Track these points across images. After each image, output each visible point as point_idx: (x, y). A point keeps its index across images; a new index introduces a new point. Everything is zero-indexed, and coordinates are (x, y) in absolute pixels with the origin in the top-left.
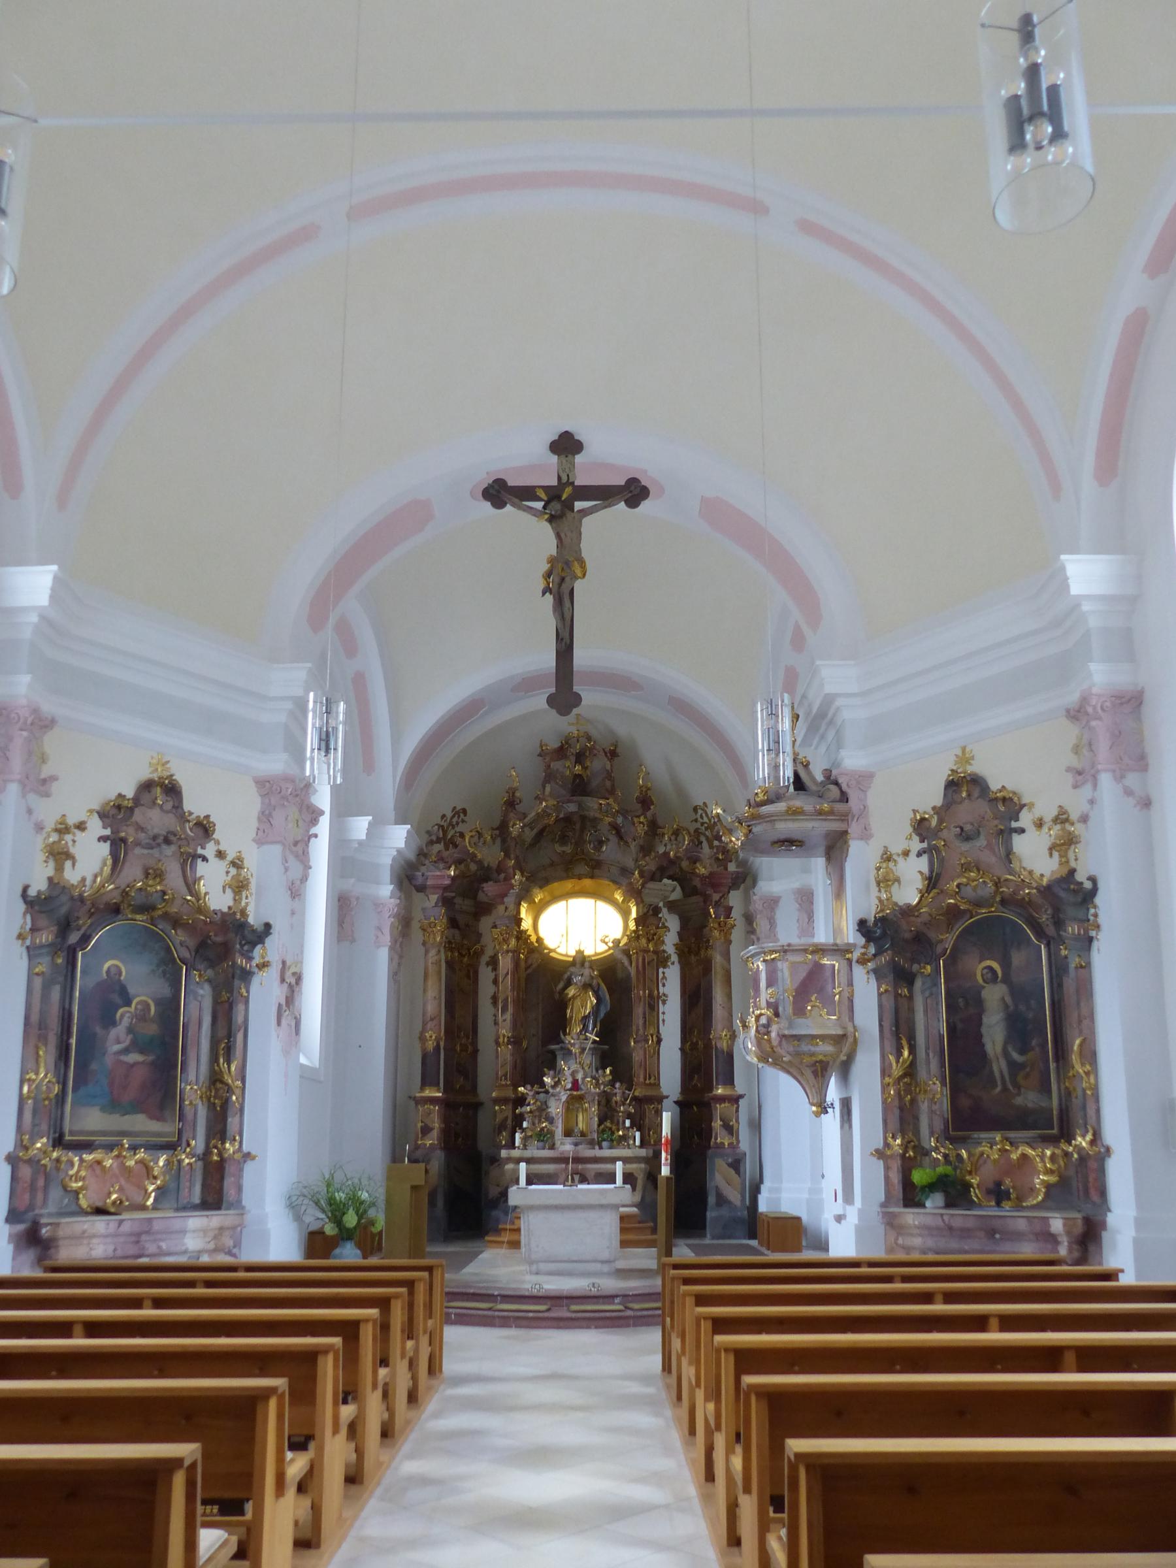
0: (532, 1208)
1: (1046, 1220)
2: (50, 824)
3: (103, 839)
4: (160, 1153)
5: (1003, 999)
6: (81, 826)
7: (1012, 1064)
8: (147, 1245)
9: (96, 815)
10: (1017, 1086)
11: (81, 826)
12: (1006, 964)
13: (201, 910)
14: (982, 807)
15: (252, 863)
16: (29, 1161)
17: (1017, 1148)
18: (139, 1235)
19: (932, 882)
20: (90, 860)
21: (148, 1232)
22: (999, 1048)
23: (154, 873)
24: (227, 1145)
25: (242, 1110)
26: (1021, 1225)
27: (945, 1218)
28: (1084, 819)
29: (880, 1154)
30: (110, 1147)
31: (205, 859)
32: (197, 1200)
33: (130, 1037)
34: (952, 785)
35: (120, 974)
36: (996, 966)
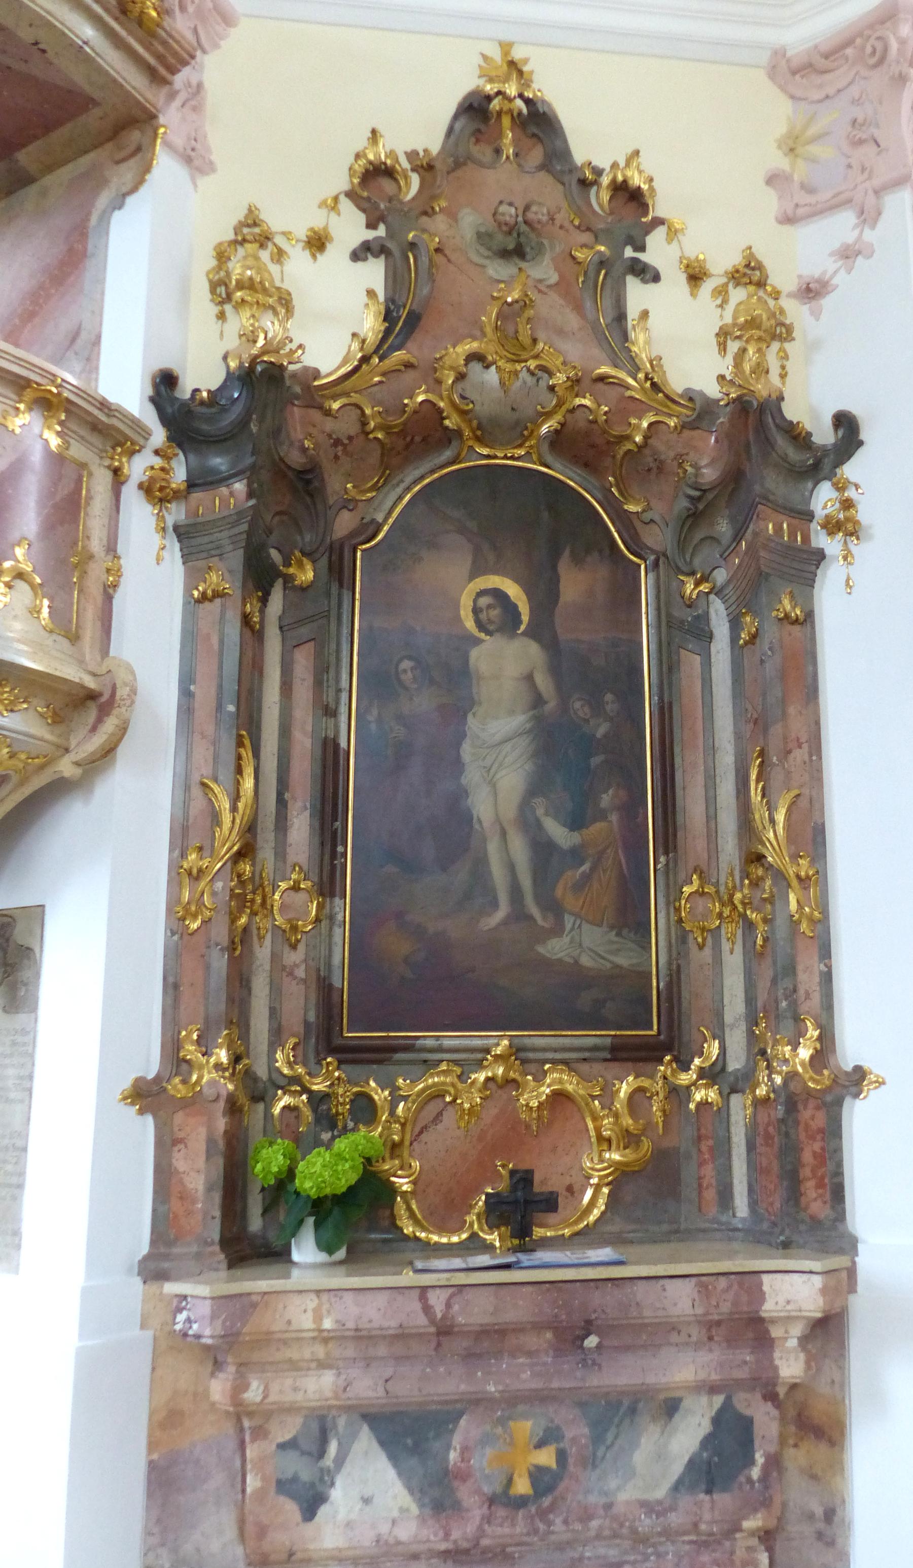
1: (749, 1281)
3: (361, 253)
5: (529, 678)
7: (543, 851)
10: (554, 908)
12: (545, 595)
14: (547, 196)
17: (539, 1078)
19: (402, 319)
20: (331, 317)
22: (509, 811)
26: (681, 1300)
27: (437, 1300)
28: (812, 291)
29: (144, 1095)
34: (476, 110)
36: (513, 590)
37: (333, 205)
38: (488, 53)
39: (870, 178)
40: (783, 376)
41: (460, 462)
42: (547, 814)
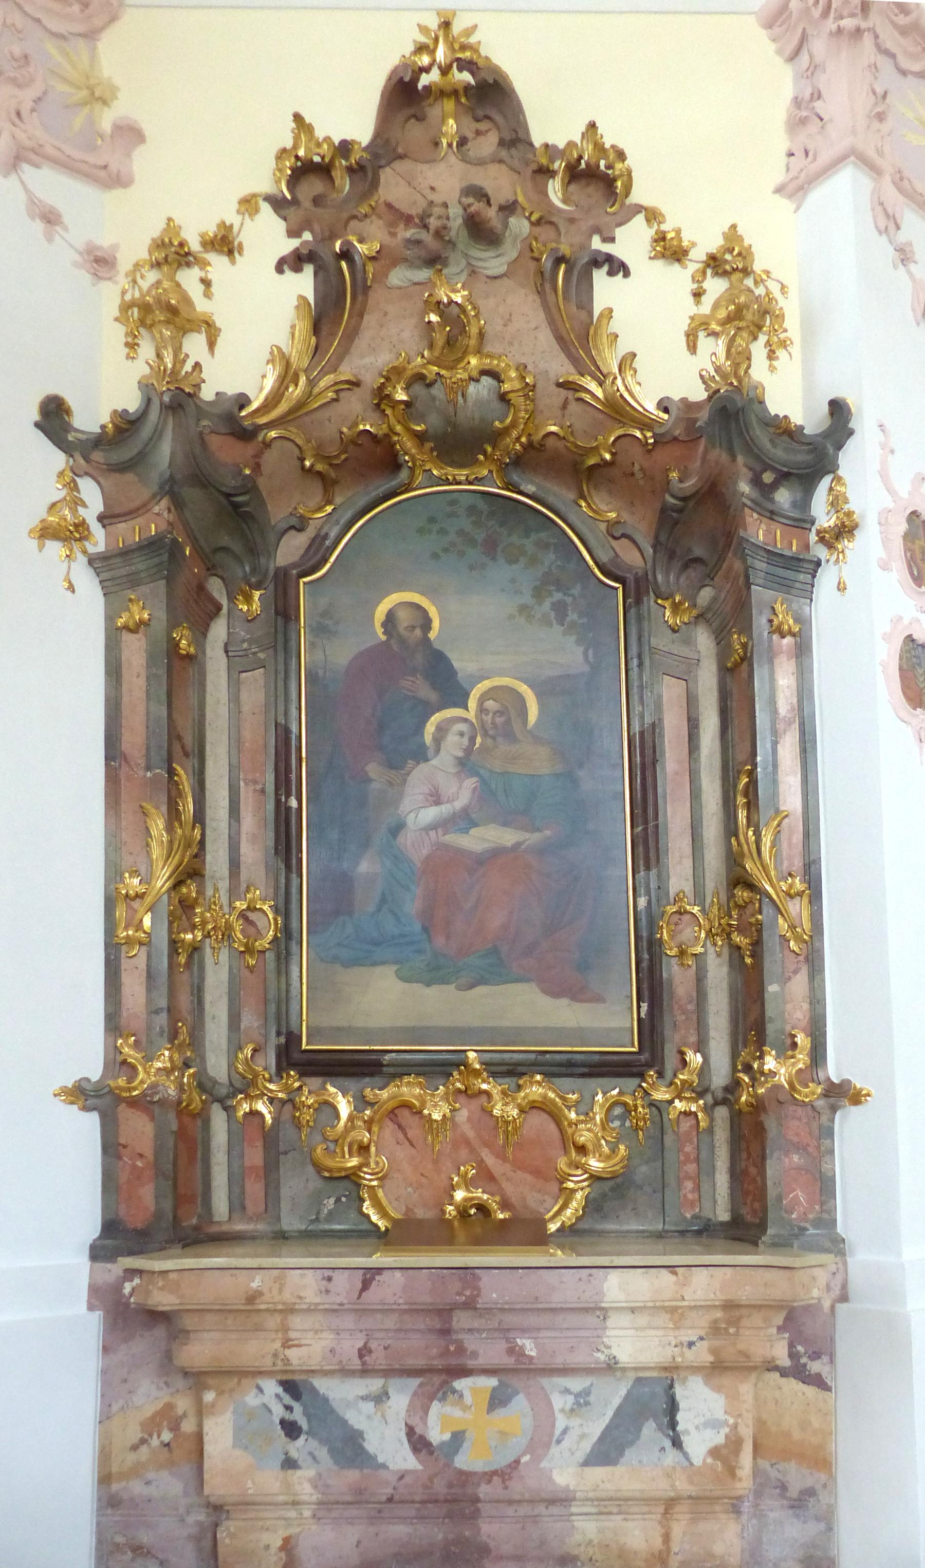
0: (462, 10)
2: (134, 248)
3: (293, 262)
4: (593, 1082)
6: (225, 243)
8: (471, 1343)
9: (266, 208)
11: (225, 243)
13: (618, 410)
15: (782, 248)
16: (140, 1103)
18: (444, 1312)
20: (253, 330)
21: (470, 1305)
23: (454, 333)
24: (770, 1063)
25: (813, 961)
30: (438, 1069)
31: (617, 267)
32: (724, 1216)
33: (471, 783)
35: (427, 624)
37: (248, 204)
38: (424, 23)
39: (815, 159)
40: (293, 327)
41: (415, 489)
42: (545, 1096)
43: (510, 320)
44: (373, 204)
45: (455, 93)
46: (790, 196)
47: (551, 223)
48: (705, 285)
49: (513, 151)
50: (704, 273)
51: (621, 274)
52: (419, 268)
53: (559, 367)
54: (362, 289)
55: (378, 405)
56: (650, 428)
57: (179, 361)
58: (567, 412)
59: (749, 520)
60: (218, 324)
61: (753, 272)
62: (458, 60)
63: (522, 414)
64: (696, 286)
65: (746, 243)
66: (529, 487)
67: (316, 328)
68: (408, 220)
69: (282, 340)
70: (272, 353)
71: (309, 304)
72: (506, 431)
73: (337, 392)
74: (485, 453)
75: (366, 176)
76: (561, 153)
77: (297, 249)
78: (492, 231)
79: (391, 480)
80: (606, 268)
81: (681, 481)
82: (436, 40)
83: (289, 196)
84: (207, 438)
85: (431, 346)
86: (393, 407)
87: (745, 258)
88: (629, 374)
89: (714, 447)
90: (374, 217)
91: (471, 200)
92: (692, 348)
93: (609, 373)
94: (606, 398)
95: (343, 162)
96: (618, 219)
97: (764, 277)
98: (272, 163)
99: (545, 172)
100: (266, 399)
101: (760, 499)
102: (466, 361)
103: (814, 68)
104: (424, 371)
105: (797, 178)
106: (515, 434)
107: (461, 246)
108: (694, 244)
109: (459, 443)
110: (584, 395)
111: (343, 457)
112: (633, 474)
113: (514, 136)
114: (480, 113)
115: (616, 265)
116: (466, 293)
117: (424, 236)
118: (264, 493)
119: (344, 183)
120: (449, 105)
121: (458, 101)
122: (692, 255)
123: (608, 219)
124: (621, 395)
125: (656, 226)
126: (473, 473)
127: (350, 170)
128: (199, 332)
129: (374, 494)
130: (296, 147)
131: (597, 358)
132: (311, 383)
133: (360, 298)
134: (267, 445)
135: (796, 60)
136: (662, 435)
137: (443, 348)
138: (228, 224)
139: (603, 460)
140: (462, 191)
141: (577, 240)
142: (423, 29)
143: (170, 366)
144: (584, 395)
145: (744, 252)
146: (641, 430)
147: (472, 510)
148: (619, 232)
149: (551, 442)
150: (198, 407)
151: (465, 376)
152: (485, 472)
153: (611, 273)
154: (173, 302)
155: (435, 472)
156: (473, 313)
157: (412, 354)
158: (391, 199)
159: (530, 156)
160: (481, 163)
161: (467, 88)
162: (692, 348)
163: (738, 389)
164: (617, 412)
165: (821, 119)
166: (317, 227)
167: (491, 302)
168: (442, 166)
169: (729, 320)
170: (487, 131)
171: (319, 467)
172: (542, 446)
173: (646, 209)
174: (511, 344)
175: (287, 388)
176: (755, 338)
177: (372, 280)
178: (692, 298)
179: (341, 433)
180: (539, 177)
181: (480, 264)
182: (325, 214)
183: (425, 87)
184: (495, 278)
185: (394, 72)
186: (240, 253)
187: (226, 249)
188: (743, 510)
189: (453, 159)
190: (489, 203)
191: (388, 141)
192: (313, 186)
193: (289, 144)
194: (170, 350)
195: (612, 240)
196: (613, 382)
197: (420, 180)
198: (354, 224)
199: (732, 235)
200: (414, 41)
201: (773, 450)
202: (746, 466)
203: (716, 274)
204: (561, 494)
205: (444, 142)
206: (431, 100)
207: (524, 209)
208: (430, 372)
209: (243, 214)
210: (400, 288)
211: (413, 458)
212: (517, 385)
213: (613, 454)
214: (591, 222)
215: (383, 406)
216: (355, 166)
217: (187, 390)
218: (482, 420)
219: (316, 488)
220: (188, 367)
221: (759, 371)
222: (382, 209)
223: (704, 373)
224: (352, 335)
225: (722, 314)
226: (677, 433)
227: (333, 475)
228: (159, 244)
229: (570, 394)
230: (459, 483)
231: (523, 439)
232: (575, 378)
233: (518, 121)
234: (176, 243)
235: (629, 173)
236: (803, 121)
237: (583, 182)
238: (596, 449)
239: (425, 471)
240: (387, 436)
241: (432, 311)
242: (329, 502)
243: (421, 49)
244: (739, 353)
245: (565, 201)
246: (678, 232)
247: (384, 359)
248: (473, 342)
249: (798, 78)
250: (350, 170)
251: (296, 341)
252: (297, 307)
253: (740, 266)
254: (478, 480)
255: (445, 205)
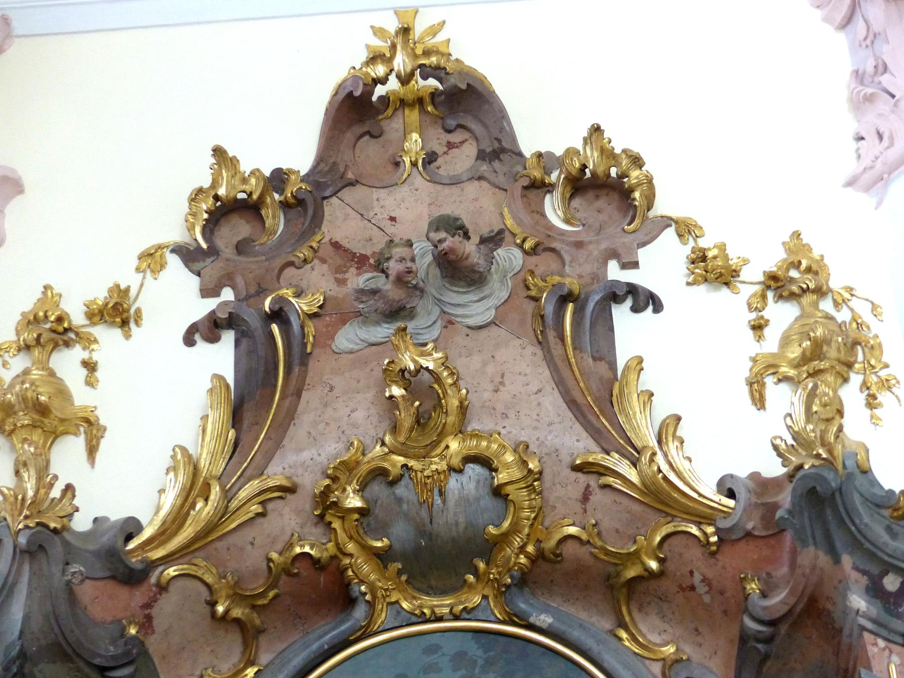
3: (209, 329)
6: (118, 312)
9: (174, 262)
11: (118, 312)
13: (662, 498)
23: (425, 407)
31: (645, 300)
37: (151, 260)
39: (891, 144)
40: (205, 418)
43: (502, 383)
44: (314, 245)
45: (420, 101)
46: (868, 189)
47: (552, 250)
48: (766, 314)
49: (496, 164)
50: (764, 297)
51: (651, 308)
52: (377, 323)
53: (577, 444)
54: (299, 358)
55: (322, 517)
56: (711, 521)
57: (45, 479)
58: (589, 506)
59: (872, 650)
60: (102, 422)
61: (831, 291)
62: (421, 66)
63: (526, 513)
64: (753, 315)
65: (816, 254)
66: (542, 617)
67: (236, 417)
68: (361, 261)
69: (189, 439)
70: (174, 457)
71: (228, 386)
72: (505, 538)
73: (261, 503)
74: (475, 572)
75: (306, 211)
76: (559, 162)
77: (213, 312)
78: (472, 270)
79: (342, 622)
80: (629, 302)
81: (764, 595)
82: (393, 47)
83: (204, 246)
84: (76, 589)
85: (395, 429)
86: (342, 518)
87: (816, 273)
88: (672, 446)
89: (805, 544)
90: (316, 261)
91: (442, 235)
92: (759, 401)
93: (645, 447)
94: (643, 483)
95: (276, 196)
96: (641, 237)
97: (847, 295)
98: (185, 207)
99: (539, 187)
100: (164, 523)
101: (886, 618)
102: (443, 445)
103: (873, 38)
104: (386, 465)
105: (872, 168)
106: (517, 541)
107: (431, 290)
108: (746, 262)
109: (437, 561)
110: (610, 480)
111: (271, 594)
112: (693, 588)
113: (496, 145)
114: (452, 123)
115: (642, 298)
116: (440, 355)
117: (380, 282)
118: (156, 660)
119: (276, 222)
120: (413, 116)
121: (422, 110)
122: (744, 275)
123: (627, 239)
124: (665, 478)
125: (691, 243)
126: (461, 603)
127: (285, 205)
128: (76, 434)
129: (315, 647)
130: (215, 184)
131: (626, 427)
132: (228, 495)
133: (296, 369)
134: (162, 588)
135: (849, 27)
136: (730, 530)
137: (411, 430)
138: (122, 287)
139: (647, 569)
140: (430, 224)
141: (588, 269)
142: (378, 32)
143: (30, 493)
144: (610, 480)
145: (815, 267)
146: (698, 524)
147: (459, 659)
148: (643, 255)
149: (570, 549)
150: (66, 543)
151: (443, 466)
152: (477, 599)
153: (636, 309)
154: (43, 398)
155: (405, 605)
156: (450, 381)
157: (368, 441)
158: (338, 237)
159: (519, 168)
160: (455, 182)
161: (434, 95)
162: (759, 401)
163: (829, 463)
164: (663, 502)
165: (893, 96)
166: (240, 281)
167: (476, 361)
168: (403, 191)
169: (805, 359)
170: (463, 142)
171: (237, 613)
172: (557, 556)
173: (676, 222)
174: (505, 416)
175: (193, 506)
176: (846, 380)
177: (313, 345)
178: (751, 332)
179: (270, 560)
180: (532, 194)
181: (459, 311)
182: (251, 265)
183: (381, 98)
184: (480, 328)
185: (340, 86)
186: (137, 324)
187: (118, 320)
188: (861, 636)
189: (419, 181)
190: (467, 236)
191: (335, 164)
192: (237, 229)
193: (206, 183)
194: (32, 472)
195: (635, 265)
196: (652, 460)
197: (377, 210)
198: (290, 272)
199: (796, 245)
200: (368, 47)
201: (893, 544)
202: (856, 568)
203: (780, 297)
204: (591, 621)
205: (407, 160)
206: (390, 111)
207: (514, 235)
208: (394, 465)
209: (144, 271)
210: (351, 352)
211: (373, 589)
212: (517, 474)
213: (661, 561)
214: (604, 245)
215: (328, 518)
216: (292, 201)
217: (52, 525)
218: (470, 525)
219: (233, 642)
220: (56, 493)
221: (856, 425)
222: (327, 251)
223: (778, 442)
224: (287, 418)
225: (794, 353)
226: (750, 526)
227: (258, 622)
228: (32, 320)
229: (592, 480)
230: (440, 619)
231: (530, 549)
232: (599, 457)
233: (502, 129)
234: (52, 318)
235: (650, 181)
236: (870, 99)
237: (591, 194)
238: (637, 553)
239: (390, 604)
240: (333, 558)
241: (396, 382)
242: (251, 663)
243: (374, 58)
244: (825, 405)
245: (567, 221)
246: (722, 247)
247: (330, 451)
248: (451, 419)
249: (856, 47)
250: (285, 205)
251: (207, 439)
252: (211, 391)
253: (812, 286)
254: (468, 613)
255: (409, 244)
